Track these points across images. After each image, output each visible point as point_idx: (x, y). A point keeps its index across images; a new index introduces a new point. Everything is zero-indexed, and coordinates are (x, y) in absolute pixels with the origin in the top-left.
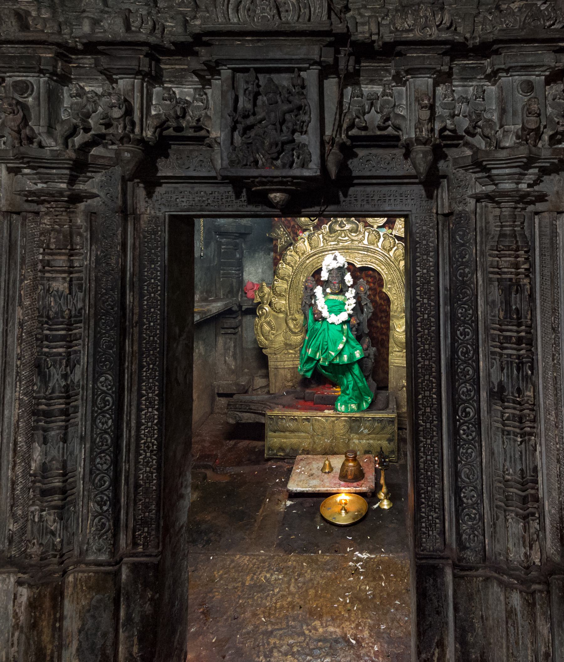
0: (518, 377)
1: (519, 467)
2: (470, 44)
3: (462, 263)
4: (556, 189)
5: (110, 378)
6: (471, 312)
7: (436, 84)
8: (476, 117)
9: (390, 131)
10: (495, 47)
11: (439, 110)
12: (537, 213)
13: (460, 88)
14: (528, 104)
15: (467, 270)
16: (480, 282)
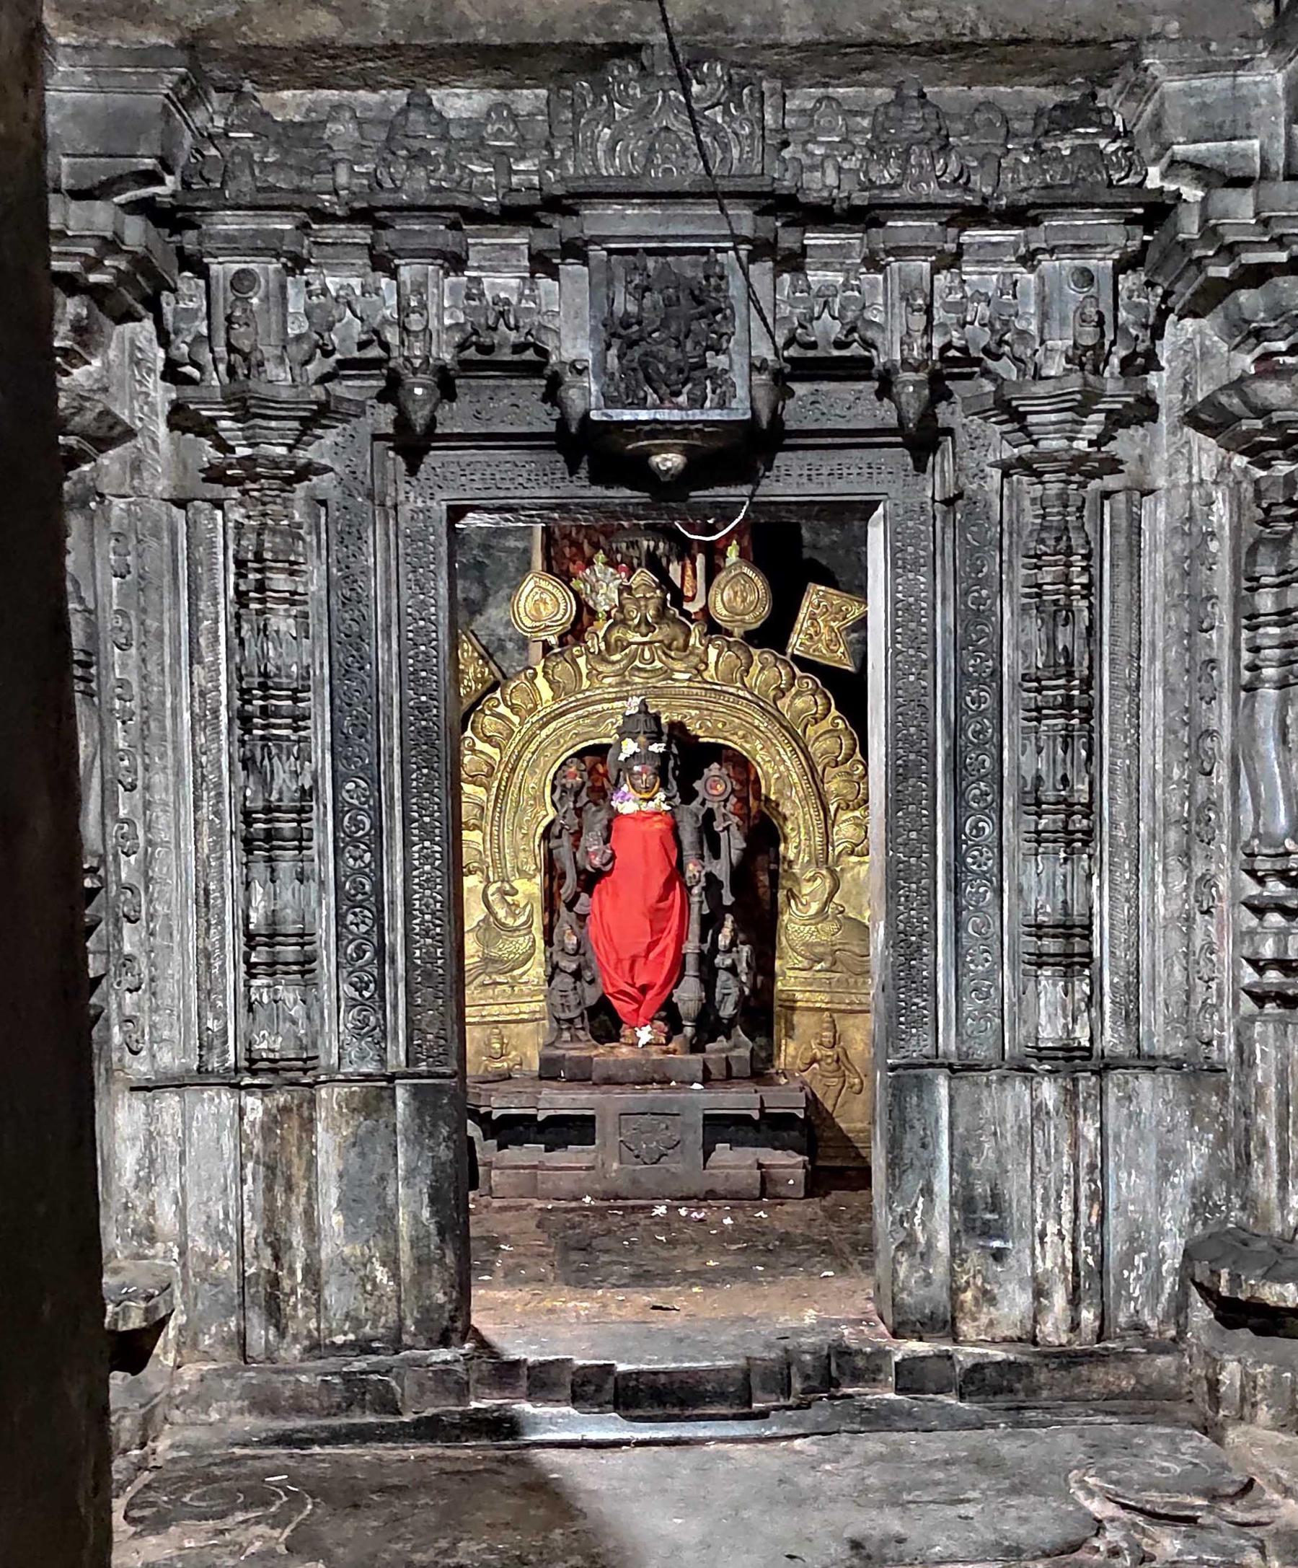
0: (1064, 761)
1: (1061, 898)
2: (992, 205)
3: (979, 582)
4: (1138, 451)
5: (363, 784)
6: (990, 663)
7: (935, 270)
8: (1000, 326)
9: (855, 350)
10: (1032, 213)
11: (939, 315)
12: (1107, 495)
13: (975, 277)
14: (1082, 307)
15: (984, 592)
16: (1007, 616)
